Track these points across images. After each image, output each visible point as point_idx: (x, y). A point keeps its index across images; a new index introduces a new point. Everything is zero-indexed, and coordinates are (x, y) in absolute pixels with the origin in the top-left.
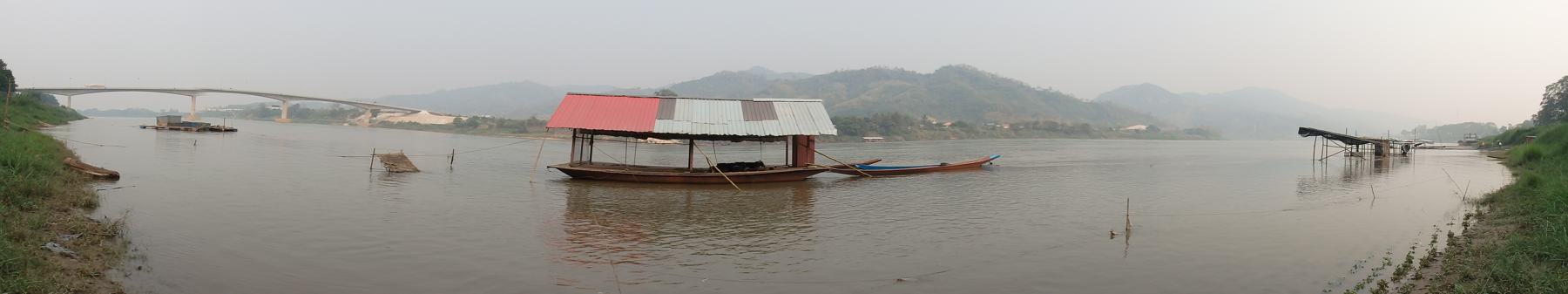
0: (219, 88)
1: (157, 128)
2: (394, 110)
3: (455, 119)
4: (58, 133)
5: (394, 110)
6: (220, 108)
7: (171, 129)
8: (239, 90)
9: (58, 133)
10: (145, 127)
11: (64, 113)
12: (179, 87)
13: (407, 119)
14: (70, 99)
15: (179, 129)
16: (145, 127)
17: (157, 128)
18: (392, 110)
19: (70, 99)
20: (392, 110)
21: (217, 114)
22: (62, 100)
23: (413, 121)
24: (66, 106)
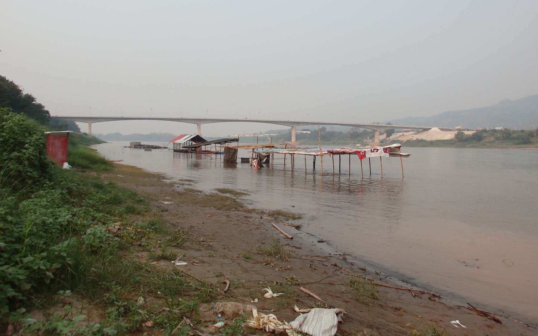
0: (235, 118)
1: (130, 147)
2: (408, 129)
3: (456, 136)
4: (94, 147)
5: (408, 129)
6: (261, 133)
7: (135, 147)
8: (252, 119)
9: (94, 147)
10: (126, 147)
11: (86, 139)
12: (184, 117)
13: (415, 137)
14: (90, 126)
15: (137, 148)
16: (126, 147)
17: (130, 147)
18: (407, 130)
19: (90, 126)
20: (407, 130)
21: (150, 137)
22: (83, 127)
23: (420, 139)
24: (88, 133)
